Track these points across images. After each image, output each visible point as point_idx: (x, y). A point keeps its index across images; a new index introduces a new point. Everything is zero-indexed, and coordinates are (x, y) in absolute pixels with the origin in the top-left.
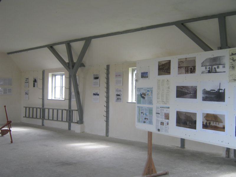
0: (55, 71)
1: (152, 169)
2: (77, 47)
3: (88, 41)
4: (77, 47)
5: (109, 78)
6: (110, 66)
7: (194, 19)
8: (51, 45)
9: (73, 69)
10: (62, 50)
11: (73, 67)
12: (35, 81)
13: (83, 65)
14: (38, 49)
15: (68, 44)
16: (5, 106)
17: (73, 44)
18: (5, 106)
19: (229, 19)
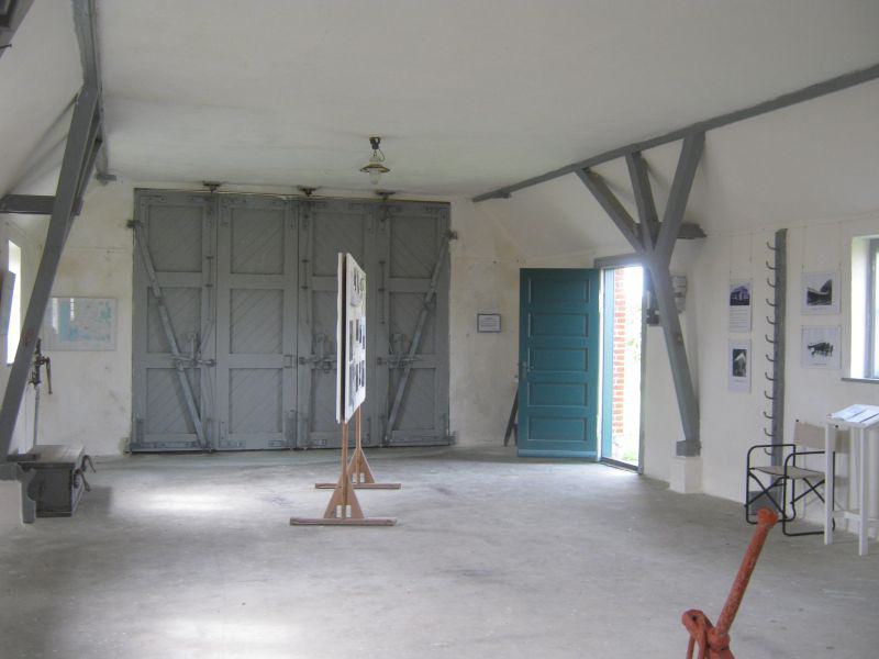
0: (615, 262)
1: (39, 341)
2: (665, 160)
3: (693, 139)
4: (665, 160)
5: (783, 336)
6: (788, 232)
7: (610, 153)
8: (584, 162)
9: (654, 248)
10: (617, 173)
11: (654, 238)
12: (738, 369)
13: (694, 231)
14: (555, 181)
15: (635, 155)
16: (50, 392)
17: (649, 155)
18: (50, 392)
19: (713, 137)
